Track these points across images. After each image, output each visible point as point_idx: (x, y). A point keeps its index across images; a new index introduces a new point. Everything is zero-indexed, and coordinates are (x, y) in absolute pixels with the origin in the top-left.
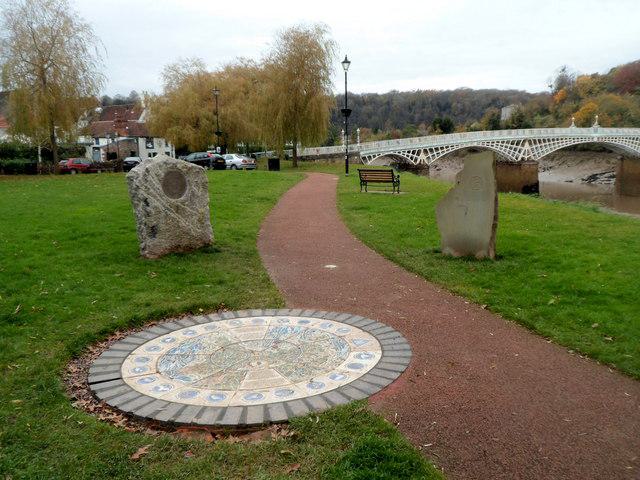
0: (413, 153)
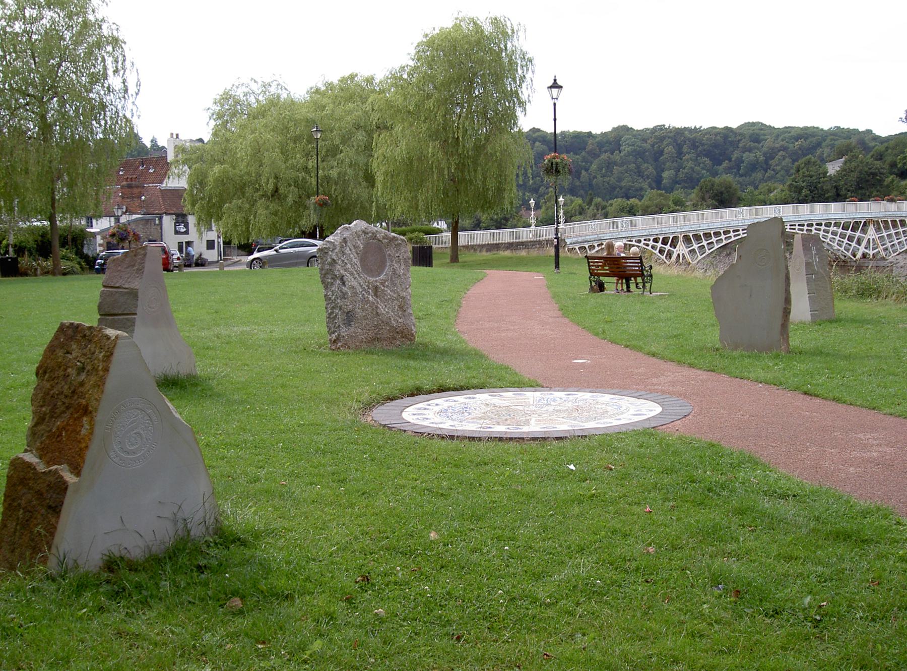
0: (665, 242)
